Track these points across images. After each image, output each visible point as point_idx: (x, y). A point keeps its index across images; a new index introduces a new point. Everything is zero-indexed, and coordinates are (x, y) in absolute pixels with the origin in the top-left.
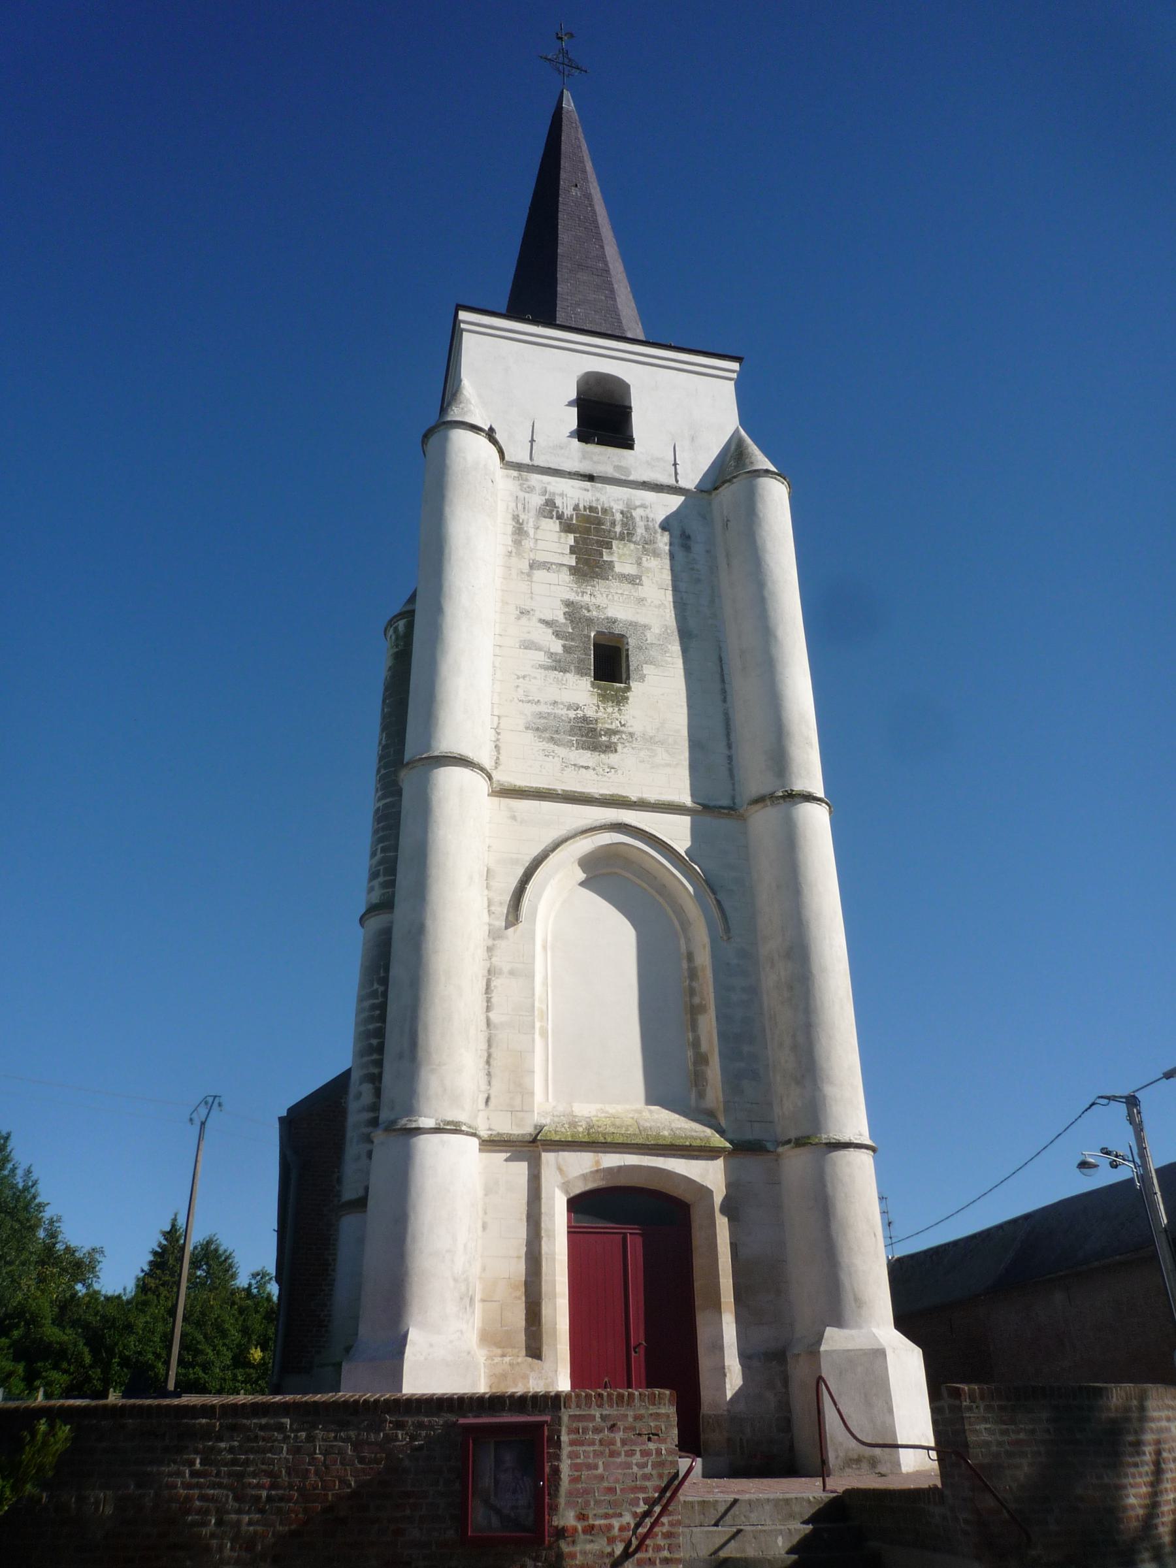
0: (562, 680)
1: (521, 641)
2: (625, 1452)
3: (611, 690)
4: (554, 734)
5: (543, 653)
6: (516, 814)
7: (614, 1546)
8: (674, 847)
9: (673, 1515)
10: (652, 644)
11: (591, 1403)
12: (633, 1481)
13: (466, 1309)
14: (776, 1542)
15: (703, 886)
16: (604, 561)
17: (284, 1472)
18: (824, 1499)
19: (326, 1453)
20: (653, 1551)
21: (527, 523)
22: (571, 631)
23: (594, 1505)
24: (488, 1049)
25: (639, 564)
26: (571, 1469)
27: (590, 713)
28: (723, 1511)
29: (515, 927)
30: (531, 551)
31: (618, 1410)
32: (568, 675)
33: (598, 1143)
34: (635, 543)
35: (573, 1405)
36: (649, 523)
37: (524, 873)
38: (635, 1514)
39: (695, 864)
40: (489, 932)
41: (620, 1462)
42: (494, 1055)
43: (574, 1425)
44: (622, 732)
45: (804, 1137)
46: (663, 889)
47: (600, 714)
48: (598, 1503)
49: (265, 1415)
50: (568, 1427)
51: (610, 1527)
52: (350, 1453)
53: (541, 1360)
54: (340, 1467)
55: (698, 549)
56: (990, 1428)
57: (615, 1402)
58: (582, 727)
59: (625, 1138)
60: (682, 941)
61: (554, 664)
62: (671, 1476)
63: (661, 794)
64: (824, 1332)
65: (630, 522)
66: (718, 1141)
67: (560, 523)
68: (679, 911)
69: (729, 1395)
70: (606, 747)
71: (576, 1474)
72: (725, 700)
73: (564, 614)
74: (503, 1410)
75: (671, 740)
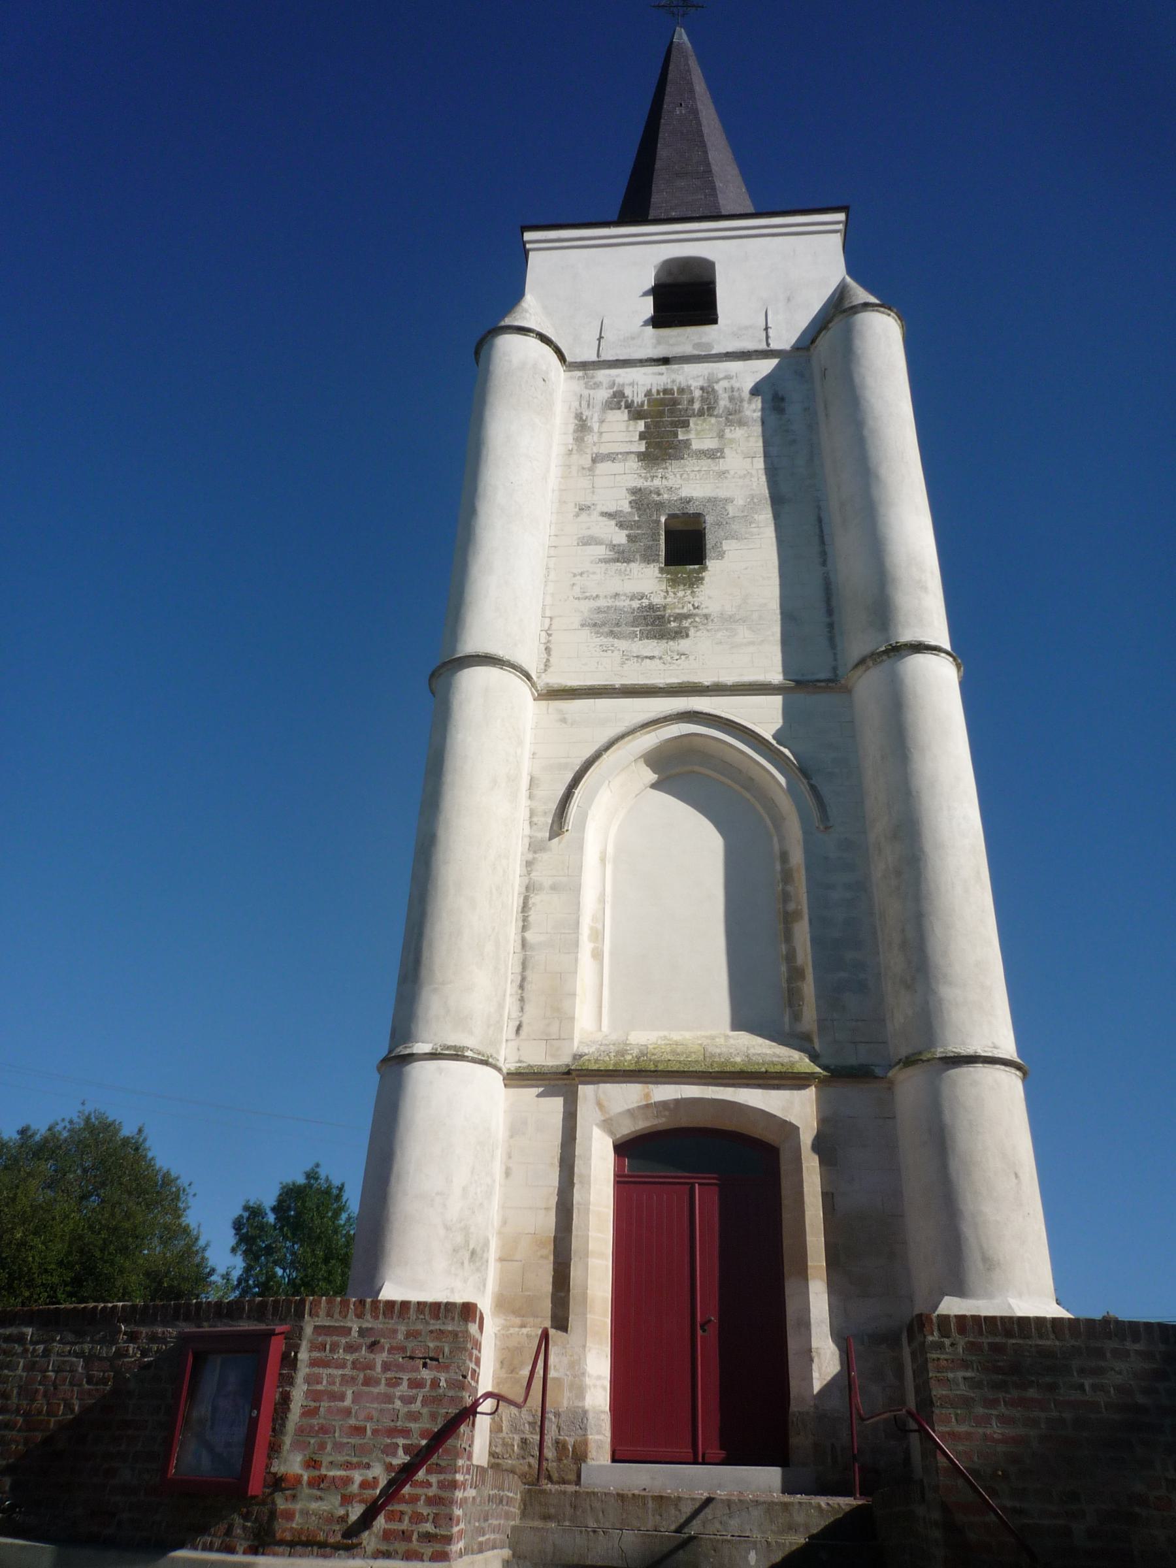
0: (626, 570)
1: (579, 538)
2: (387, 1379)
3: (682, 573)
5: (604, 546)
6: (566, 716)
7: (350, 1509)
8: (756, 731)
9: (446, 1473)
10: (734, 517)
13: (462, 1263)
14: (746, 1558)
15: (796, 774)
16: (679, 441)
17: (15, 1392)
18: (843, 1507)
19: (57, 1371)
20: (410, 1521)
21: (592, 418)
22: (637, 518)
23: (333, 1448)
25: (721, 436)
26: (306, 1398)
27: (657, 600)
28: (689, 1514)
30: (595, 445)
31: (384, 1323)
32: (632, 565)
33: (646, 1071)
34: (716, 416)
35: (322, 1313)
36: (734, 393)
38: (389, 1467)
39: (785, 747)
41: (378, 1393)
42: (529, 979)
43: (320, 1339)
44: (696, 615)
45: (916, 1054)
46: (749, 782)
47: (669, 600)
48: (338, 1446)
50: (311, 1342)
51: (348, 1481)
52: (80, 1370)
54: (68, 1387)
55: (794, 409)
56: (972, 1378)
57: (381, 1311)
60: (775, 839)
61: (616, 556)
62: (449, 1417)
63: (742, 675)
64: (939, 1304)
65: (711, 396)
67: (629, 412)
69: (817, 1386)
70: (676, 633)
71: (313, 1404)
72: (824, 563)
73: (630, 502)
74: (241, 1318)
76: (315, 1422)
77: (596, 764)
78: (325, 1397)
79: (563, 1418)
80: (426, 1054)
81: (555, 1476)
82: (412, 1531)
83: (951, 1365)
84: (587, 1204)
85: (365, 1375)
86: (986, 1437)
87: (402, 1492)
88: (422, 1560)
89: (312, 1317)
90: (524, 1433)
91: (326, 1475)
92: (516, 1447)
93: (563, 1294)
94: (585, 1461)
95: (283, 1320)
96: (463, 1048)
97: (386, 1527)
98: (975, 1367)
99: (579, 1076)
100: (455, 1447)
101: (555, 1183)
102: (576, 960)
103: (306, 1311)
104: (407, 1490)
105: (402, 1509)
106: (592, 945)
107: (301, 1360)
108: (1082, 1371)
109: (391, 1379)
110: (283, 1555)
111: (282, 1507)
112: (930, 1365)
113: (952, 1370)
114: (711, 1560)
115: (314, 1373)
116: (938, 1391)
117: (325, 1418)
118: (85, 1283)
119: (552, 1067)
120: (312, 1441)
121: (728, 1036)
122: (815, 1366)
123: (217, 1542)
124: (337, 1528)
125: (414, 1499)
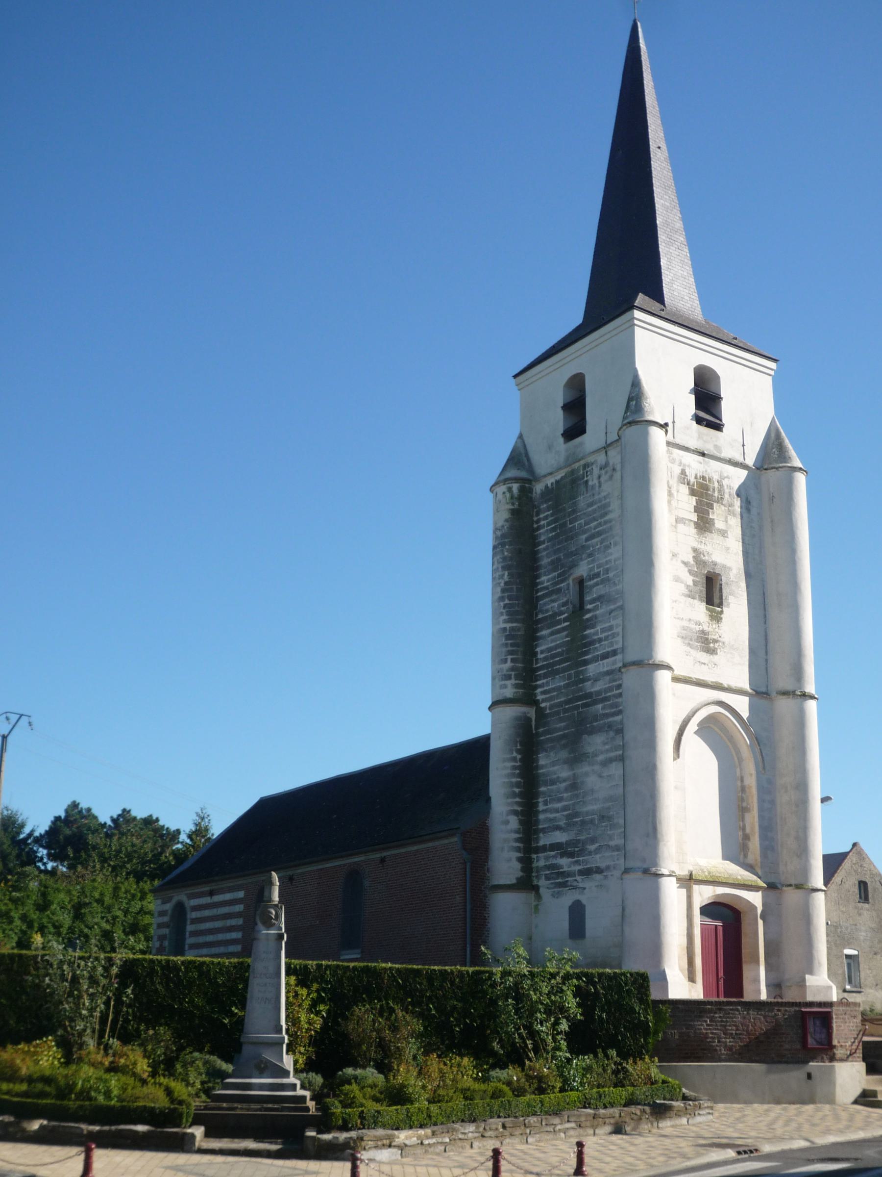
19: (754, 1019)
34: (725, 506)
49: (731, 1005)
55: (754, 511)
60: (738, 770)
66: (762, 884)
68: (738, 752)
72: (765, 623)
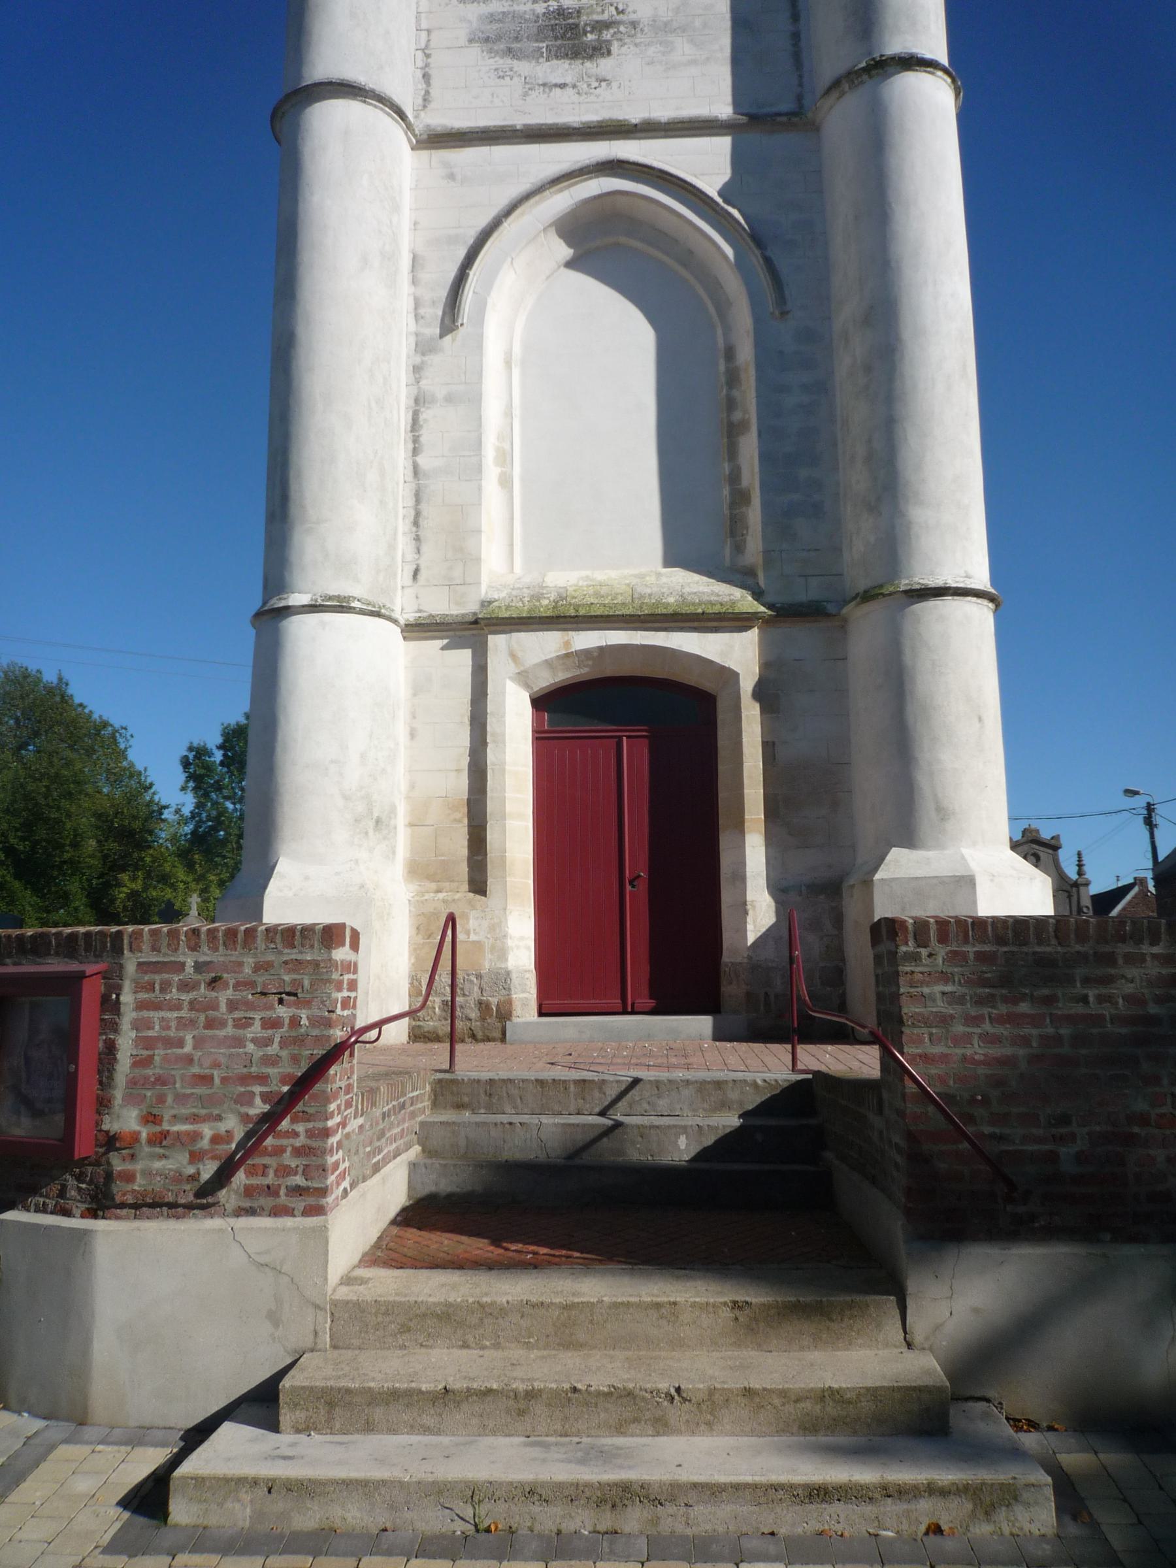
2: (234, 1020)
4: (513, 43)
7: (201, 1167)
9: (315, 1121)
11: (179, 944)
12: (245, 1066)
13: (367, 833)
18: (781, 1083)
24: (417, 505)
26: (136, 1046)
28: (614, 1096)
29: (454, 332)
31: (226, 955)
33: (565, 617)
37: (466, 254)
38: (245, 1118)
39: (734, 207)
40: (416, 345)
41: (225, 1036)
42: (425, 513)
43: (146, 978)
45: (875, 587)
48: (181, 1099)
51: (196, 1136)
53: (486, 896)
57: (221, 942)
58: (556, 25)
59: (608, 609)
60: (719, 332)
68: (714, 287)
69: (751, 938)
70: (594, 49)
71: (146, 1053)
74: (49, 954)
75: (698, 23)
76: (149, 1072)
77: (495, 235)
78: (160, 1045)
79: (486, 979)
80: (303, 606)
81: (480, 1035)
82: (279, 1186)
83: (927, 979)
84: (502, 765)
85: (207, 1017)
86: (964, 1058)
87: (264, 1144)
88: (294, 1216)
89: (134, 953)
90: (445, 995)
91: (168, 1131)
92: (437, 1009)
93: (480, 858)
94: (509, 1020)
95: (98, 957)
96: (348, 599)
97: (247, 1182)
98: (956, 979)
99: (487, 625)
100: (324, 1092)
101: (467, 742)
102: (480, 489)
103: (125, 947)
104: (269, 1141)
105: (264, 1162)
106: (498, 470)
107: (125, 1004)
108: (1086, 981)
109: (240, 1019)
110: (127, 1218)
111: (119, 1169)
112: (902, 980)
113: (928, 984)
114: (638, 1146)
115: (144, 1018)
116: (909, 1009)
117: (161, 1068)
118: (34, 828)
119: (457, 616)
120: (149, 1094)
121: (659, 573)
122: (749, 919)
123: (51, 1203)
124: (188, 1187)
125: (279, 1151)
